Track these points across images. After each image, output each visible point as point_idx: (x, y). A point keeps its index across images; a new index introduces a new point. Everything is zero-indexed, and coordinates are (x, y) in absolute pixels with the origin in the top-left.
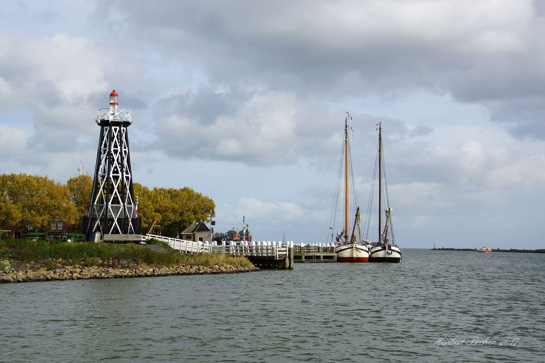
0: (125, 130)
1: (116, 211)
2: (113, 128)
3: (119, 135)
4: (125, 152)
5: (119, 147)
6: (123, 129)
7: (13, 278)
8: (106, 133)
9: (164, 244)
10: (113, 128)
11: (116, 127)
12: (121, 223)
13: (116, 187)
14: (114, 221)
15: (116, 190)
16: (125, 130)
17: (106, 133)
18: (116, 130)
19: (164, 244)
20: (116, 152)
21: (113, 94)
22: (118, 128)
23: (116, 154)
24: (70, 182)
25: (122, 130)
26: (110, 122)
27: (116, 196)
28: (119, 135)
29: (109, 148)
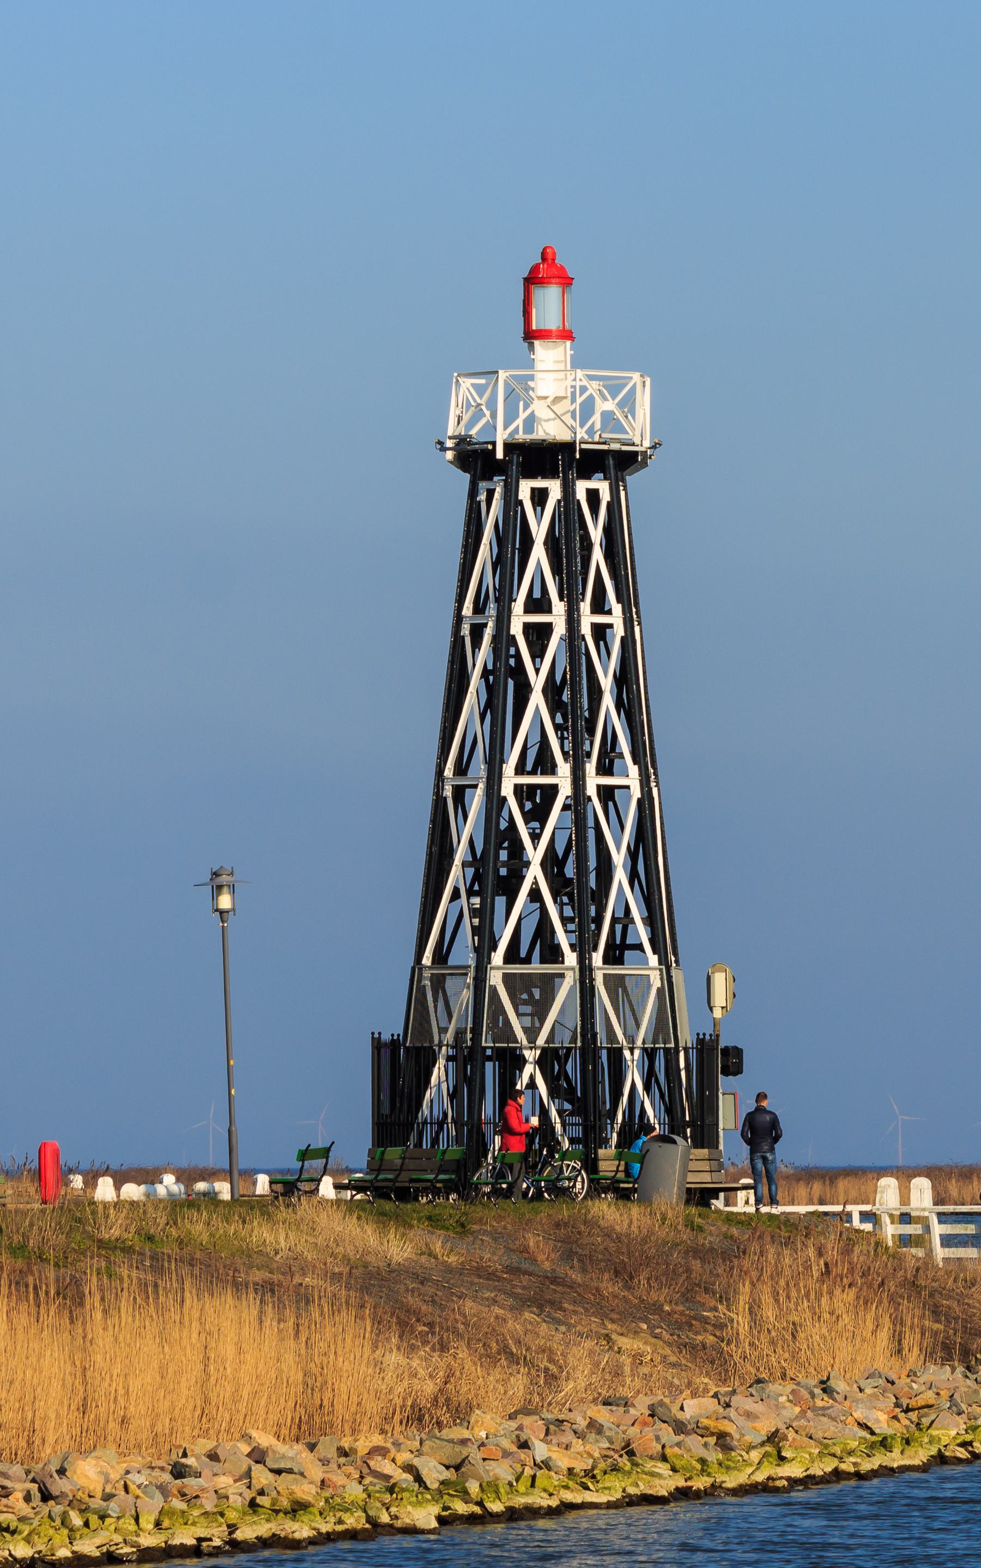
0: (605, 497)
1: (537, 648)
2: (525, 488)
3: (574, 838)
4: (607, 794)
5: (564, 768)
6: (593, 496)
7: (299, 1200)
8: (493, 514)
9: (802, 1447)
10: (525, 488)
11: (540, 483)
12: (547, 870)
13: (535, 855)
14: (522, 1061)
15: (534, 873)
16: (605, 497)
17: (493, 514)
18: (540, 497)
19: (802, 1447)
20: (538, 604)
21: (216, 874)
22: (554, 488)
23: (539, 509)
24: (465, 471)
25: (581, 495)
26: (500, 455)
27: (538, 660)
28: (574, 838)
29: (488, 778)
